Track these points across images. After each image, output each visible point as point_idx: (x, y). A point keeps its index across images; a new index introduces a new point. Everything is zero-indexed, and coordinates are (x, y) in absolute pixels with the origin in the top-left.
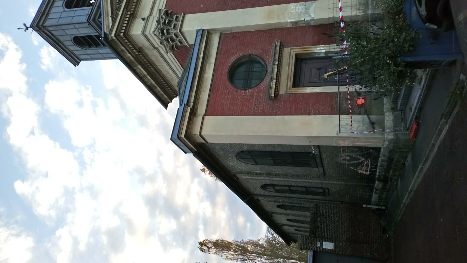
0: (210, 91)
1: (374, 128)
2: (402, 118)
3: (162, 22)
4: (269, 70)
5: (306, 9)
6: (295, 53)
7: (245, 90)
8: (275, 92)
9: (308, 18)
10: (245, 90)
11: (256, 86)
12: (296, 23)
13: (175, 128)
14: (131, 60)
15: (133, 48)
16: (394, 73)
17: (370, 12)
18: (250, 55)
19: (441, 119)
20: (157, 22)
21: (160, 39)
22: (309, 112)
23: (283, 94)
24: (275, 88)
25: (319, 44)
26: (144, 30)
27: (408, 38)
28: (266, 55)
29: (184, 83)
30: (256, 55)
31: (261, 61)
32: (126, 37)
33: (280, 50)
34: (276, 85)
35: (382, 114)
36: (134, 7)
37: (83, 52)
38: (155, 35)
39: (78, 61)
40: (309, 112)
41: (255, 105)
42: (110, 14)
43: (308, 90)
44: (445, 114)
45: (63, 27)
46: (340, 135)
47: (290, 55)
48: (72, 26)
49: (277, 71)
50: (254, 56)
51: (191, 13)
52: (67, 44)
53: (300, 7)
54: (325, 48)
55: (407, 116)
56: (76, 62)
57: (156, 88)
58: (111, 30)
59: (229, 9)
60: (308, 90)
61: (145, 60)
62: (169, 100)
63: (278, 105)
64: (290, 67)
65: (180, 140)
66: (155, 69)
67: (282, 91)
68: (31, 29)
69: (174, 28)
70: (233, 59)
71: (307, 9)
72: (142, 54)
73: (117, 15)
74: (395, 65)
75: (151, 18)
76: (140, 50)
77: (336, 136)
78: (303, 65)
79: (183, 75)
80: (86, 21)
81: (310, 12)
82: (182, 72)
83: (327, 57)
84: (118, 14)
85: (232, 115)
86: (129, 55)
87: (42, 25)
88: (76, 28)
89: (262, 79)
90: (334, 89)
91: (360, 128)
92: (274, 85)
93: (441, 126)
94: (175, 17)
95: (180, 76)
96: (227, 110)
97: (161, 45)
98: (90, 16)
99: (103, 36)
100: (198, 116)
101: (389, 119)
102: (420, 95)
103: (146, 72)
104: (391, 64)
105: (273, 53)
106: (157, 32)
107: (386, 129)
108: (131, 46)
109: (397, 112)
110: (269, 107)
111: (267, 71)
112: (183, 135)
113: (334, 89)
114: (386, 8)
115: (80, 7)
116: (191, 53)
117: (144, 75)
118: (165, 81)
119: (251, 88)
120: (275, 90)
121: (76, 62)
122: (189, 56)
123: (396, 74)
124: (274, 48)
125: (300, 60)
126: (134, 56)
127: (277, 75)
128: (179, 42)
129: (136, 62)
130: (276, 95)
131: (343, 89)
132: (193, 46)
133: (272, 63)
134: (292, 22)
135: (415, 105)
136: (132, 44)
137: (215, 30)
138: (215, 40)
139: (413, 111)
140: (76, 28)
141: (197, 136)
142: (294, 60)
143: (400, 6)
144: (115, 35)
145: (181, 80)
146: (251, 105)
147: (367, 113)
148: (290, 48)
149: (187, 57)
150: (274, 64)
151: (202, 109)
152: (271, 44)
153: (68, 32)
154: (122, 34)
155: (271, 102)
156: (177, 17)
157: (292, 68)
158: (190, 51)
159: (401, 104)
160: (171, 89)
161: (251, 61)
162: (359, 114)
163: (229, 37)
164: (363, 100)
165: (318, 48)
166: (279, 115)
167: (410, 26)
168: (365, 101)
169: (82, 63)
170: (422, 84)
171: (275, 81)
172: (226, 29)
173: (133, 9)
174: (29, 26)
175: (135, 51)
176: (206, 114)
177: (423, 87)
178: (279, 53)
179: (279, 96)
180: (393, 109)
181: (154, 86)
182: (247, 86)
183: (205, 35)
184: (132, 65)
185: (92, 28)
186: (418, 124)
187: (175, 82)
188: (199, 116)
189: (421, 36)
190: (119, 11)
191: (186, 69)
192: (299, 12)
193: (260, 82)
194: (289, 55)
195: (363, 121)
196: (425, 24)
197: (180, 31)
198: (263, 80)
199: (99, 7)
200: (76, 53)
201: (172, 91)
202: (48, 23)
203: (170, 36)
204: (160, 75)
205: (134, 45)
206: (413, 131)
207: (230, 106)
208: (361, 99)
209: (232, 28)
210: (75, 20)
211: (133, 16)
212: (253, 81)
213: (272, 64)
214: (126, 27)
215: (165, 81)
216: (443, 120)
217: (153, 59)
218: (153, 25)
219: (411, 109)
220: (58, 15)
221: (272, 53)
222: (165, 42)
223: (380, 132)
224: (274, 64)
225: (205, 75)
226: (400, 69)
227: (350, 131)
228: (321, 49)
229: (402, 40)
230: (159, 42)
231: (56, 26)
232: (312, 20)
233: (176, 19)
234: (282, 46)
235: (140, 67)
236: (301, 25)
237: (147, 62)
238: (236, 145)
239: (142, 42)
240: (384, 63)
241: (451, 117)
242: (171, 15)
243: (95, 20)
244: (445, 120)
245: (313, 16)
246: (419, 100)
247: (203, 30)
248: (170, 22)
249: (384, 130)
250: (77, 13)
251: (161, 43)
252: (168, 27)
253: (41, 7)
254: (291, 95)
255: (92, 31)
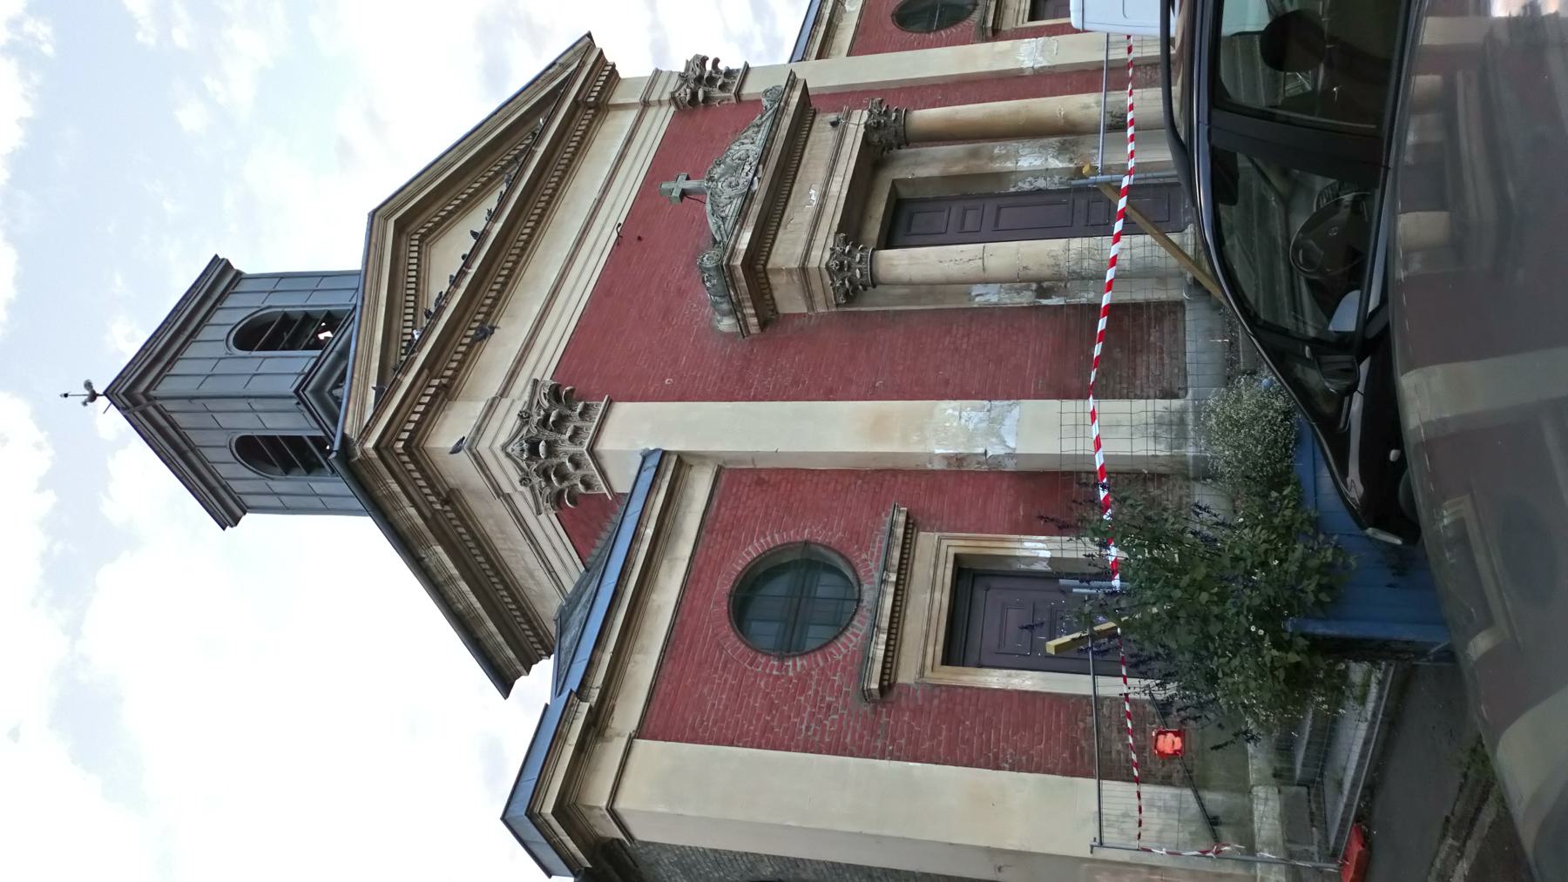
0: (664, 651)
1: (1217, 839)
2: (1312, 813)
3: (536, 418)
4: (868, 597)
5: (992, 421)
6: (952, 551)
7: (782, 659)
8: (883, 673)
9: (995, 450)
10: (782, 659)
11: (820, 648)
12: (960, 459)
13: (522, 784)
14: (414, 526)
15: (427, 491)
16: (1273, 669)
17: (1190, 451)
18: (806, 543)
19: (1444, 836)
20: (520, 416)
21: (522, 469)
22: (996, 757)
23: (908, 686)
24: (885, 662)
25: (1030, 530)
26: (478, 431)
27: (1313, 563)
28: (860, 549)
29: (579, 614)
30: (827, 547)
31: (840, 563)
32: (411, 455)
33: (905, 538)
34: (887, 650)
35: (1246, 791)
36: (454, 365)
37: (260, 485)
38: (508, 455)
39: (238, 511)
40: (996, 757)
41: (812, 715)
42: (373, 383)
43: (995, 679)
44: (1453, 820)
45: (212, 405)
46: (1102, 854)
47: (937, 557)
48: (242, 405)
49: (894, 605)
50: (822, 550)
51: (632, 399)
52: (210, 455)
53: (973, 414)
54: (1051, 546)
55: (1328, 806)
56: (226, 511)
57: (481, 622)
58: (367, 430)
59: (754, 399)
60: (995, 679)
61: (462, 530)
62: (520, 667)
63: (892, 722)
64: (937, 595)
65: (536, 826)
66: (488, 560)
67: (907, 675)
68: (103, 401)
69: (571, 439)
70: (752, 551)
71: (995, 422)
72: (455, 510)
73: (396, 384)
74: (1277, 644)
75: (506, 402)
76: (451, 497)
77: (1089, 855)
78: (979, 593)
79: (580, 588)
80: (291, 391)
81: (1003, 431)
82: (577, 578)
83: (1058, 572)
84: (400, 383)
85: (731, 744)
86: (412, 511)
87: (145, 393)
88: (254, 411)
89: (841, 626)
90: (1078, 685)
91: (1171, 836)
92: (880, 652)
93: (1444, 862)
94: (581, 405)
95: (569, 588)
96: (715, 722)
97: (521, 488)
98: (307, 377)
99: (337, 446)
100: (610, 740)
101: (1266, 810)
102: (1366, 742)
103: (457, 567)
104: (1262, 638)
105: (884, 545)
106: (514, 448)
107: (1258, 846)
108: (422, 483)
109: (1294, 789)
110: (858, 726)
111: (859, 600)
112: (548, 809)
113: (1078, 685)
114: (1239, 461)
115: (283, 349)
116: (616, 518)
117: (451, 577)
118: (515, 601)
119: (802, 654)
120: (884, 668)
121: (226, 511)
122: (610, 528)
123: (1281, 674)
124: (887, 527)
125: (969, 576)
126: (429, 515)
127: (892, 617)
128: (583, 482)
129: (429, 535)
130: (887, 687)
131: (1111, 687)
132: (625, 499)
133: (877, 575)
134: (946, 457)
135: (1351, 773)
136: (426, 478)
137: (701, 457)
138: (700, 488)
139: (1346, 792)
140: (254, 411)
141: (597, 812)
142: (949, 573)
143: (1281, 461)
144: (376, 447)
145: (572, 602)
146: (797, 715)
147: (1193, 781)
148: (937, 535)
149: (603, 529)
150: (883, 581)
151: (628, 712)
152: (878, 514)
153: (224, 420)
154: (401, 444)
155: (868, 708)
156: (586, 407)
157: (943, 598)
158: (615, 512)
159: (1306, 757)
160: (533, 628)
161: (809, 563)
162: (1166, 781)
163: (742, 482)
164: (1178, 740)
165: (1027, 544)
166: (893, 757)
167: (1316, 524)
168: (1183, 742)
169: (248, 520)
170: (1370, 706)
171: (884, 637)
172: (738, 457)
173: (449, 373)
174: (99, 389)
175: (432, 498)
176: (642, 732)
177: (1374, 715)
178: (903, 548)
179: (895, 690)
180: (1281, 776)
181: (478, 616)
182: (789, 647)
183: (670, 469)
184: (415, 543)
185: (307, 414)
186: (1366, 841)
187: (549, 605)
188: (616, 740)
189: (1352, 561)
190: (405, 374)
191: (593, 569)
192: (971, 427)
193: (836, 638)
194: (936, 554)
195: (1180, 810)
196: (1364, 528)
197: (591, 450)
198: (846, 628)
199: (343, 354)
200: (237, 486)
201: (537, 635)
202: (167, 387)
203: (555, 461)
204: (503, 581)
205: (432, 477)
206: (1351, 864)
207: (726, 707)
208: (1170, 736)
209: (754, 456)
210: (259, 386)
211: (447, 393)
212: (813, 631)
213: (877, 580)
214: (418, 423)
215: (515, 601)
216: (1450, 841)
217: (489, 526)
218: (506, 424)
219: (1340, 784)
220: (206, 367)
221: (880, 541)
222: (537, 481)
223: (1238, 856)
224: (883, 581)
225: (654, 596)
226: (1293, 658)
227: (1135, 844)
228: (1038, 549)
229: (1294, 568)
230: (516, 478)
231: (191, 398)
232: (1011, 456)
233: (581, 414)
234: (911, 526)
235: (439, 549)
236: (974, 467)
237: (466, 537)
238: (735, 856)
239: (461, 471)
240: (1242, 632)
241: (1475, 836)
242: (570, 400)
243: (322, 394)
244: (1456, 844)
245: (1012, 444)
246: (1363, 756)
247: (664, 453)
248: (562, 420)
249: (1251, 850)
250: (267, 366)
251: (524, 481)
252: (553, 436)
253: (155, 336)
254: (937, 691)
255: (305, 425)
